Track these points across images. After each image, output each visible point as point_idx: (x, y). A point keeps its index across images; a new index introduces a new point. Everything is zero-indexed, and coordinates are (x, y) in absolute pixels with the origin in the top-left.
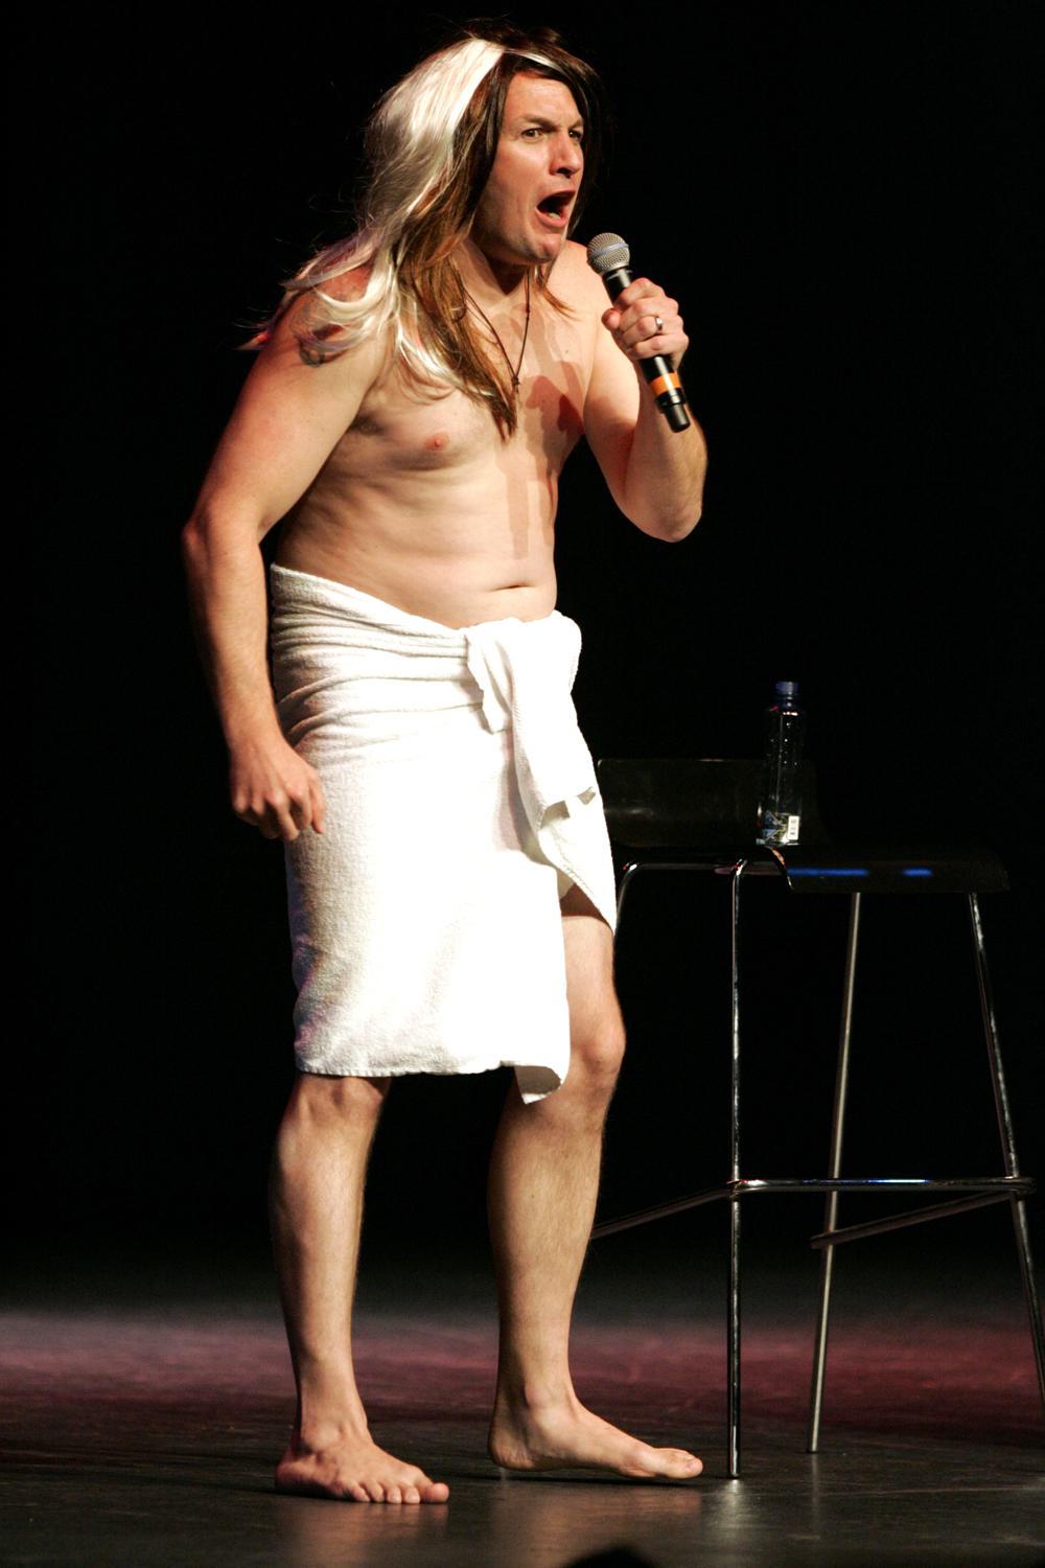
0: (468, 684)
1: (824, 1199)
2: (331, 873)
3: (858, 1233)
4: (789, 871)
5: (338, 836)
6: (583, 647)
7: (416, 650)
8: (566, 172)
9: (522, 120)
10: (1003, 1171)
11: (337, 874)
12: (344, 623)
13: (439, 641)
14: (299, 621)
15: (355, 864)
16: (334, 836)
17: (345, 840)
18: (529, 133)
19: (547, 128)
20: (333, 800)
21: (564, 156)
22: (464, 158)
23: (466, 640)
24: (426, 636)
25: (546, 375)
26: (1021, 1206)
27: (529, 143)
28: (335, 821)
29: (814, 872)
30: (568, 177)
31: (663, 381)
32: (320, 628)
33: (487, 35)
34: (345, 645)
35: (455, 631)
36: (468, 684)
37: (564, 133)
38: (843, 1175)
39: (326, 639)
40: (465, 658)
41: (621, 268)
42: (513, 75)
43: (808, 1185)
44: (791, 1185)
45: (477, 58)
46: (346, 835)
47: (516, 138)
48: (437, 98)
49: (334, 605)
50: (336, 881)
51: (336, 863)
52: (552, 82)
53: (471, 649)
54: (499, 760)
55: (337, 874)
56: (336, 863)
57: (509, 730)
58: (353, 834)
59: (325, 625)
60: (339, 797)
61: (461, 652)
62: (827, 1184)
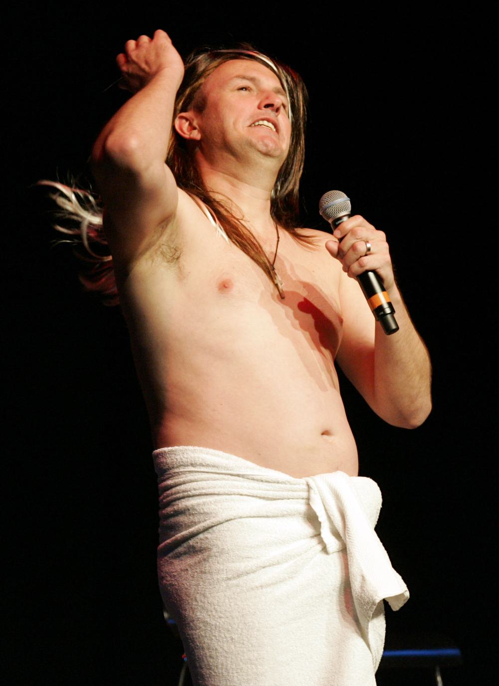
0: (312, 518)
7: (271, 494)
11: (236, 674)
12: (217, 476)
20: (223, 620)
23: (308, 485)
24: (278, 483)
31: (378, 297)
32: (198, 483)
34: (218, 494)
35: (300, 480)
36: (312, 518)
39: (204, 491)
40: (308, 499)
53: (312, 492)
56: (234, 666)
57: (344, 550)
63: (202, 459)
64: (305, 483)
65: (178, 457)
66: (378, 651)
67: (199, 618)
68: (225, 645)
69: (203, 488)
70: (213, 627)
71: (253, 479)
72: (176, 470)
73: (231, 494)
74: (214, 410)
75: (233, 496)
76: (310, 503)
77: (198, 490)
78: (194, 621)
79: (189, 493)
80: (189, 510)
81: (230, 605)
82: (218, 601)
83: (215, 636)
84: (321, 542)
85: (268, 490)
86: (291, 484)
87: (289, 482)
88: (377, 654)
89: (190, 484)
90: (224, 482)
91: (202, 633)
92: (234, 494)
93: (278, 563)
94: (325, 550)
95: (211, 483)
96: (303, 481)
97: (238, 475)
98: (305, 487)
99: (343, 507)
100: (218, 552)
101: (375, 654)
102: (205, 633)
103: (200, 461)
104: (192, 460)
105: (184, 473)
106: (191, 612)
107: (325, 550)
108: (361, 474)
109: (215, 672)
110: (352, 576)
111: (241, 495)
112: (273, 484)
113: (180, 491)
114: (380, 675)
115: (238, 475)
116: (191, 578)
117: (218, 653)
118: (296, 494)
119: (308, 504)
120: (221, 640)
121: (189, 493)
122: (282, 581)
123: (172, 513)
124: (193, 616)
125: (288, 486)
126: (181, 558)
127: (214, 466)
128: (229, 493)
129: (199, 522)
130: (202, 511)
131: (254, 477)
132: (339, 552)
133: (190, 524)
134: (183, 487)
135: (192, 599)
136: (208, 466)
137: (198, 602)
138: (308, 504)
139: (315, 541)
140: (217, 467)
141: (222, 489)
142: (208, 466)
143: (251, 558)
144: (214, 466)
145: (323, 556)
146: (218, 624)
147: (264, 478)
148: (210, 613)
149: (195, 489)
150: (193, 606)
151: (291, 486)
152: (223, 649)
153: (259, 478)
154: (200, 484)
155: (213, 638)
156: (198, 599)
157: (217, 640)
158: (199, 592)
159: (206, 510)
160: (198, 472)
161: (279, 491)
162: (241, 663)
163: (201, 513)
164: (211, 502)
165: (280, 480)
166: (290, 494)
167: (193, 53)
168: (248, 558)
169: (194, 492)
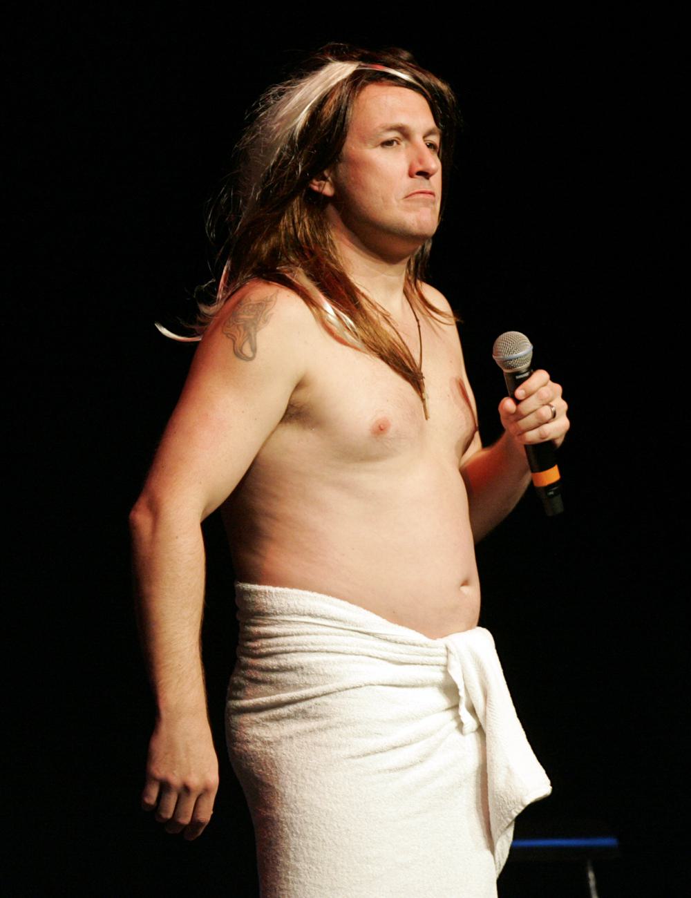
0: (450, 689)
6: (526, 733)
7: (404, 658)
8: (425, 174)
9: (380, 130)
11: (346, 875)
12: (341, 631)
13: (425, 650)
18: (388, 143)
19: (405, 133)
21: (421, 161)
22: (265, 112)
23: (447, 649)
24: (414, 645)
25: (506, 434)
30: (428, 179)
32: (319, 637)
34: (343, 653)
35: (434, 641)
36: (450, 689)
39: (325, 648)
40: (446, 666)
41: (525, 373)
47: (376, 146)
49: (334, 616)
54: (473, 762)
57: (480, 730)
59: (324, 634)
61: (443, 660)
63: (325, 610)
64: (444, 646)
65: (291, 603)
66: (503, 855)
69: (324, 644)
71: (386, 640)
73: (359, 655)
74: (343, 555)
75: (361, 657)
76: (450, 672)
77: (318, 645)
78: (296, 802)
79: (305, 647)
80: (302, 668)
82: (334, 782)
84: (457, 718)
85: (401, 653)
86: (428, 647)
87: (426, 645)
88: (501, 858)
90: (340, 639)
91: (306, 818)
92: (363, 655)
93: (410, 744)
94: (460, 726)
95: (326, 639)
96: (441, 642)
97: (368, 634)
98: (444, 651)
99: (486, 679)
100: (341, 723)
101: (499, 858)
103: (323, 612)
104: (311, 609)
107: (460, 726)
108: (482, 623)
109: (317, 868)
110: (495, 766)
111: (370, 656)
112: (409, 647)
113: (292, 644)
114: (504, 883)
115: (368, 634)
116: (299, 750)
117: (326, 845)
118: (432, 660)
119: (446, 672)
120: (332, 831)
121: (305, 647)
122: (413, 765)
123: (275, 667)
125: (425, 650)
126: (281, 722)
127: (340, 621)
128: (357, 653)
130: (322, 672)
131: (387, 637)
132: (475, 732)
133: (301, 686)
134: (296, 639)
136: (332, 619)
137: (306, 780)
138: (446, 672)
139: (449, 715)
140: (344, 622)
141: (349, 648)
142: (332, 619)
143: (381, 734)
144: (340, 621)
145: (457, 734)
147: (399, 639)
148: (322, 795)
149: (312, 644)
151: (429, 650)
153: (393, 638)
154: (320, 638)
155: (322, 826)
157: (326, 829)
158: (308, 767)
159: (326, 671)
160: (318, 624)
161: (414, 655)
164: (334, 663)
165: (417, 642)
166: (426, 659)
168: (378, 734)
169: (312, 647)
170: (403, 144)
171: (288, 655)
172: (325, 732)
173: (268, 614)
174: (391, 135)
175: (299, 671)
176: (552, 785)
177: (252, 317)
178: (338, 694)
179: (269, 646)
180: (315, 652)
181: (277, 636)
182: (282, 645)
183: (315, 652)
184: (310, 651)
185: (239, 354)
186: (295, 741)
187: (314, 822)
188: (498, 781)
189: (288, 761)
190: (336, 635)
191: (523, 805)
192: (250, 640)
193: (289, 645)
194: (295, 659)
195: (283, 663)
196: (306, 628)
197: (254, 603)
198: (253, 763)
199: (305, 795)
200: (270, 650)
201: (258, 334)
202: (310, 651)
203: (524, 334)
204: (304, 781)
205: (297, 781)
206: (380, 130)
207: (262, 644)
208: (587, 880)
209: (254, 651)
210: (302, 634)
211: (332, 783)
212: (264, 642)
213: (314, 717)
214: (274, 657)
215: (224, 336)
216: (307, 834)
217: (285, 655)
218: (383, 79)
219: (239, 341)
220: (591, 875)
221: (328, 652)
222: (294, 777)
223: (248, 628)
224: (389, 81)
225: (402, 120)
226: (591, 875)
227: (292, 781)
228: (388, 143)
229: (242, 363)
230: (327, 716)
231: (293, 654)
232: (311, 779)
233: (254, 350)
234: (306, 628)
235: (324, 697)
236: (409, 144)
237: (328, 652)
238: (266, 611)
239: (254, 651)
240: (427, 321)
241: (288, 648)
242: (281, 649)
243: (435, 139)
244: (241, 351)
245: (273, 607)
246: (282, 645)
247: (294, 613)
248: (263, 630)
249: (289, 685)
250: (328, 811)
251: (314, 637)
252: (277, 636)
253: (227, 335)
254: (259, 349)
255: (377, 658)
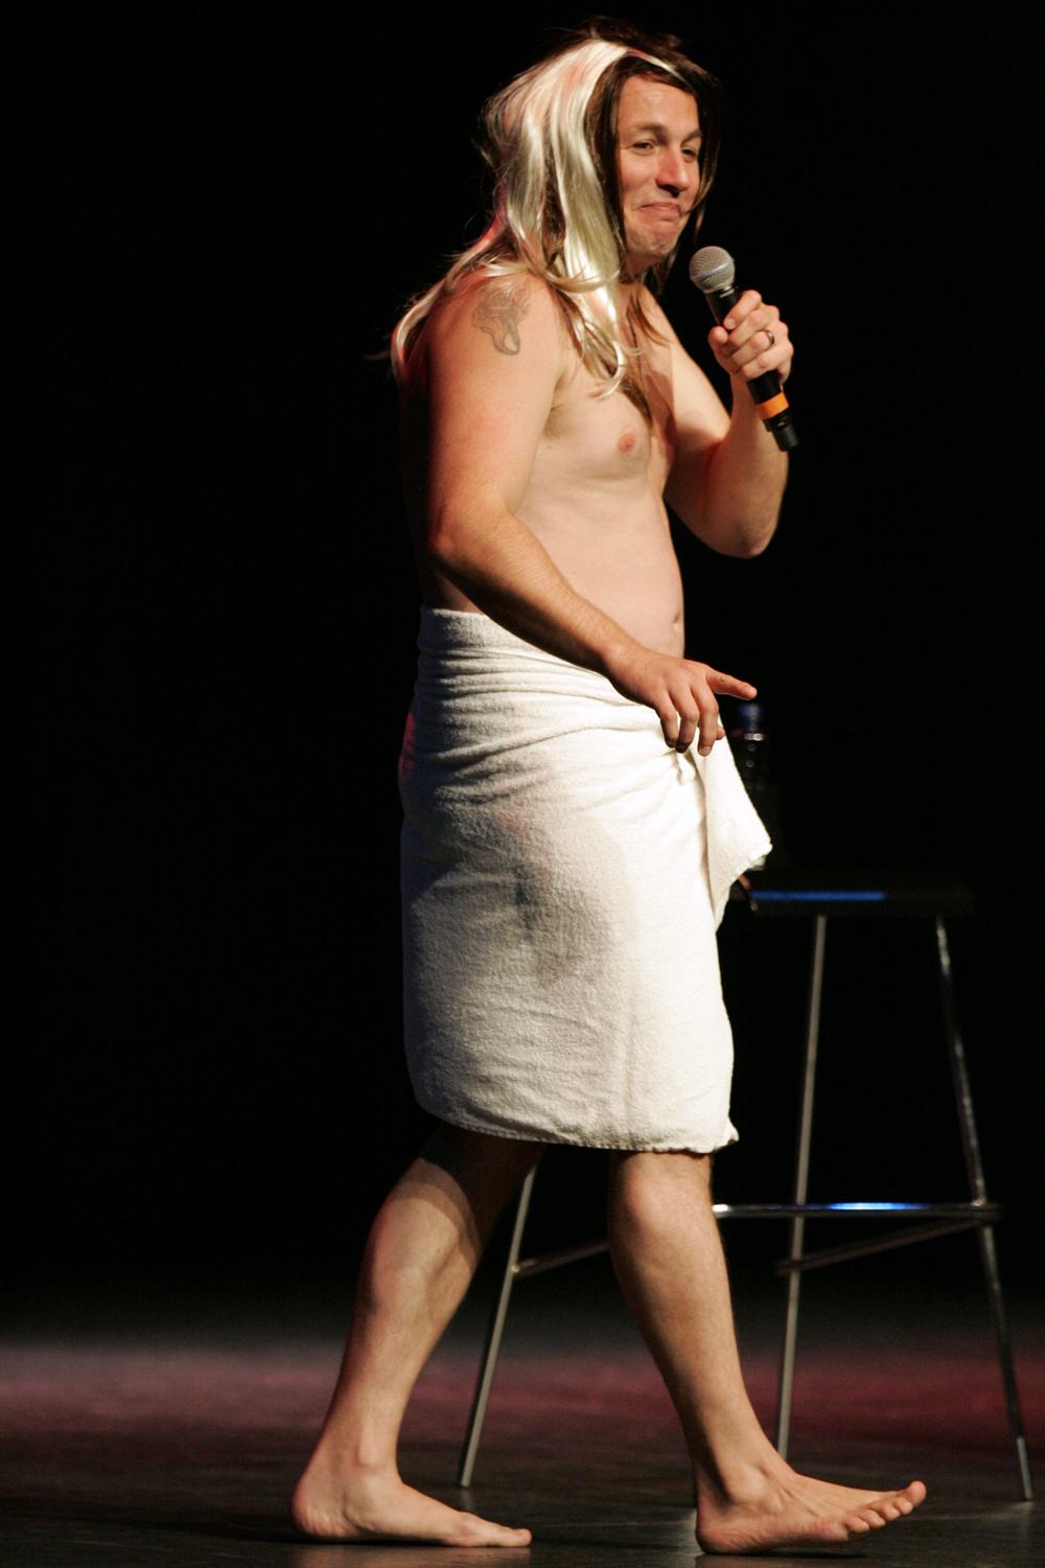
1: (786, 1226)
2: (576, 940)
3: (825, 1259)
4: (756, 895)
5: (582, 904)
10: (970, 1196)
14: (467, 654)
15: (603, 931)
16: (576, 904)
17: (589, 908)
19: (660, 136)
20: (571, 867)
21: (673, 173)
26: (988, 1233)
27: (638, 154)
28: (575, 888)
29: (777, 896)
32: (514, 674)
33: (609, 37)
37: (676, 147)
38: (810, 1199)
39: (540, 687)
42: (628, 76)
43: (774, 1210)
44: (778, 1211)
45: (600, 55)
46: (588, 902)
48: (552, 101)
50: (582, 948)
51: (581, 931)
52: (673, 89)
55: (582, 941)
56: (581, 931)
57: (698, 777)
58: (598, 900)
59: (538, 671)
60: (577, 864)
62: (792, 1211)
67: (532, 864)
68: (571, 901)
70: (555, 877)
72: (494, 650)
81: (583, 847)
83: (556, 889)
89: (520, 674)
92: (580, 696)
95: (541, 677)
102: (541, 884)
105: (498, 656)
106: (519, 854)
121: (516, 686)
124: (524, 859)
129: (529, 728)
130: (536, 714)
134: (487, 677)
135: (521, 836)
146: (562, 872)
149: (525, 682)
150: (524, 847)
152: (569, 907)
155: (554, 891)
156: (532, 837)
162: (591, 927)
163: (535, 717)
167: (786, 377)
169: (524, 686)
170: (657, 149)
171: (496, 694)
172: (546, 785)
173: (472, 645)
174: (645, 137)
175: (509, 712)
176: (772, 842)
177: (506, 308)
178: (556, 739)
179: (473, 684)
180: (527, 691)
181: (483, 672)
182: (490, 683)
183: (527, 691)
184: (522, 691)
185: (501, 348)
186: (513, 797)
187: (545, 887)
188: (720, 834)
189: (508, 821)
190: (551, 672)
191: (749, 861)
192: (445, 677)
193: (497, 683)
194: (497, 700)
195: (489, 703)
196: (518, 664)
197: (456, 632)
198: (460, 825)
199: (532, 857)
200: (474, 688)
201: (519, 327)
202: (522, 691)
203: (714, 358)
204: (529, 843)
205: (522, 843)
206: (633, 130)
207: (463, 681)
208: (936, 938)
209: (451, 689)
210: (514, 671)
211: (561, 842)
212: (465, 678)
213: (530, 769)
214: (478, 696)
215: (479, 330)
216: (538, 900)
217: (491, 695)
218: (649, 73)
219: (499, 334)
220: (941, 934)
221: (542, 692)
222: (518, 838)
223: (442, 662)
224: (655, 76)
225: (659, 118)
226: (941, 934)
227: (515, 842)
228: (642, 145)
229: (504, 358)
230: (539, 767)
231: (501, 694)
232: (538, 840)
233: (518, 343)
234: (518, 664)
235: (540, 744)
236: (664, 149)
237: (542, 692)
238: (470, 641)
239: (451, 689)
240: (644, 332)
241: (496, 687)
242: (487, 687)
243: (695, 145)
244: (504, 346)
245: (479, 636)
246: (490, 683)
247: (504, 645)
248: (464, 664)
249: (495, 730)
250: (559, 873)
251: (527, 674)
252: (483, 672)
253: (482, 328)
254: (523, 343)
255: (594, 698)
